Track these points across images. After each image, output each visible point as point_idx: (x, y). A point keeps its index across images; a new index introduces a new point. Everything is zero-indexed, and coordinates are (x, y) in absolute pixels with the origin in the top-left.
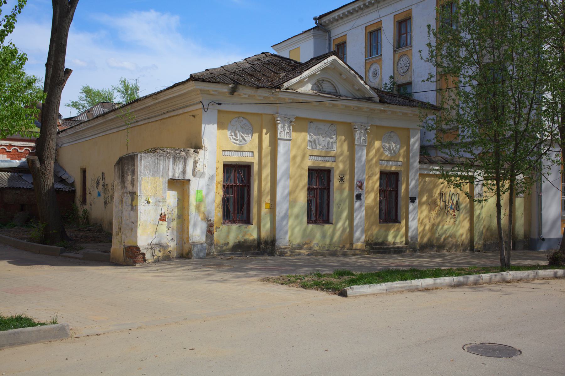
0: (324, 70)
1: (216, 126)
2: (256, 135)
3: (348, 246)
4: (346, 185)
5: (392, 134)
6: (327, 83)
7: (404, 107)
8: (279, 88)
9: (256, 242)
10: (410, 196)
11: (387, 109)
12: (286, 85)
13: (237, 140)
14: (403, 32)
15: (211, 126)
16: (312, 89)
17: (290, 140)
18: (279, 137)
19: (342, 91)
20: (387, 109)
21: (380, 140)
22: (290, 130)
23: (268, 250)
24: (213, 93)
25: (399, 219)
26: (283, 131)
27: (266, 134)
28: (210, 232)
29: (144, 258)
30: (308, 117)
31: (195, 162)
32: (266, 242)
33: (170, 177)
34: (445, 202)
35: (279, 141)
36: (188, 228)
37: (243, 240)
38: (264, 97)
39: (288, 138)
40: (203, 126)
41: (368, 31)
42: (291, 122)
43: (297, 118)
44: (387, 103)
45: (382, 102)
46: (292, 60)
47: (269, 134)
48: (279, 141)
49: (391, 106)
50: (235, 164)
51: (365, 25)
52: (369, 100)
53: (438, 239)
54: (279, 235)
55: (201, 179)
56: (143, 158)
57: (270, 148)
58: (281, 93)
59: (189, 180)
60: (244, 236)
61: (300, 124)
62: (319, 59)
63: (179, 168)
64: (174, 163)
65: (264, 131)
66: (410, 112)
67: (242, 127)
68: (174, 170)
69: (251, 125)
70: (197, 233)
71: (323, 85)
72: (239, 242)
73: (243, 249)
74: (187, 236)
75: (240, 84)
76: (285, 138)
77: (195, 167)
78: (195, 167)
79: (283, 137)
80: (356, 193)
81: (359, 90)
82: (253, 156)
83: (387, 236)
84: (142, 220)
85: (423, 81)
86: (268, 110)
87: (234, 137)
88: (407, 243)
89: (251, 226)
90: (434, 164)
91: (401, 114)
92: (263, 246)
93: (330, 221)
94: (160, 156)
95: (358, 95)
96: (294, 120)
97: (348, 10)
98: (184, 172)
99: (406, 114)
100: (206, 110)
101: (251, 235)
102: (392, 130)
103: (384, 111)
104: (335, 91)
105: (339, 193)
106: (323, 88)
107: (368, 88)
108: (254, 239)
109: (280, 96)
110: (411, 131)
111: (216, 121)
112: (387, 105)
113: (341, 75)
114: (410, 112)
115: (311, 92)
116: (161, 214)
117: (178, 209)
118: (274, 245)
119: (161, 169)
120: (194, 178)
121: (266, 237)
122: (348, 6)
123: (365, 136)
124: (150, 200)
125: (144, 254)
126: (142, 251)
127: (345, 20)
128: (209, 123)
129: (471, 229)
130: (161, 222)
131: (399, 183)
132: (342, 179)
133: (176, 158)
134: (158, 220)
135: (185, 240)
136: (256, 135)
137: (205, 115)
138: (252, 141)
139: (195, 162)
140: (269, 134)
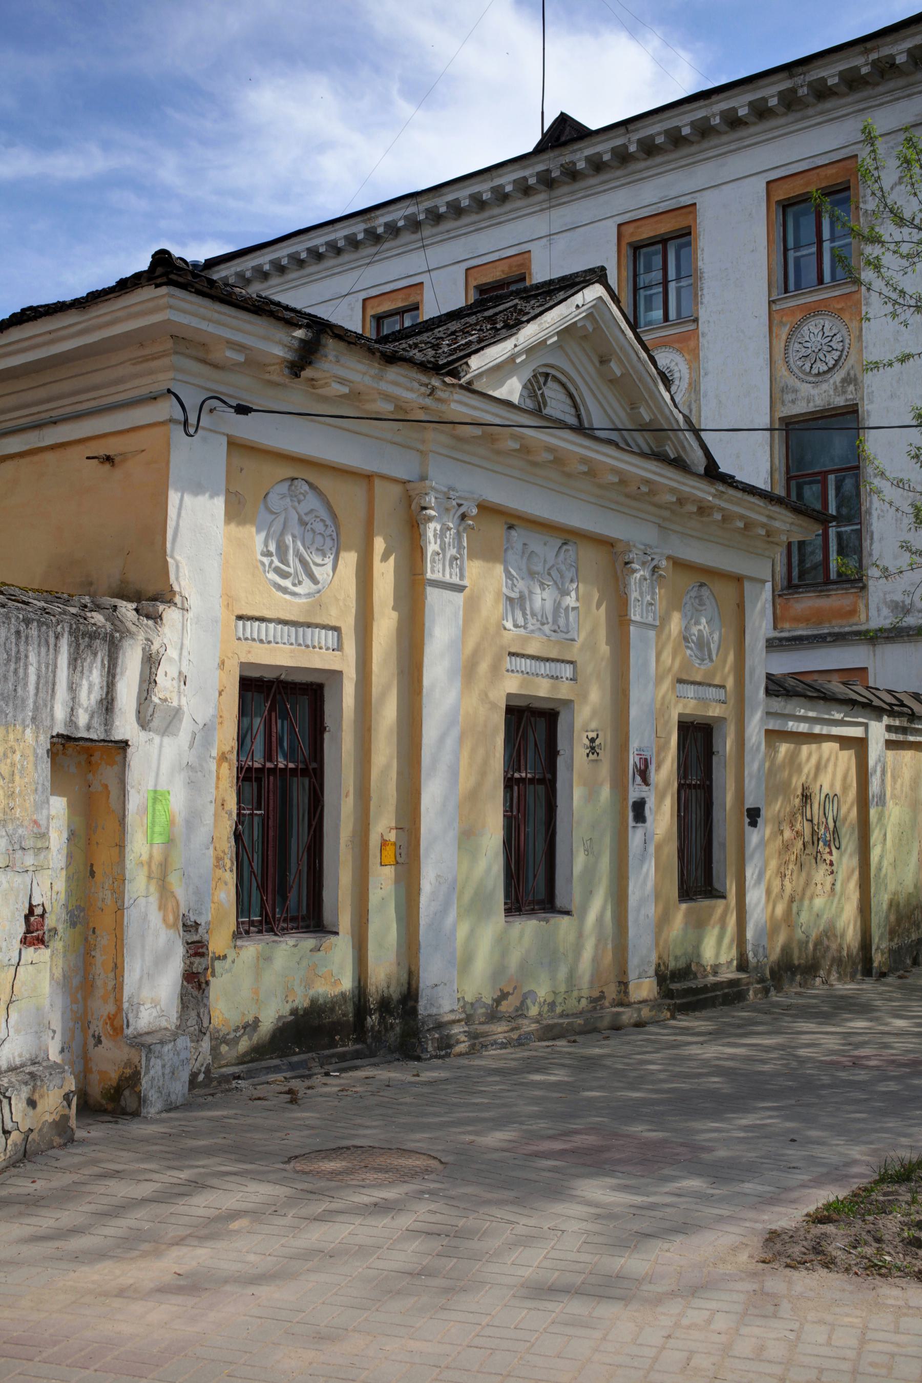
0: (568, 332)
1: (219, 503)
2: (116, 768)
3: (611, 992)
4: (605, 770)
5: (705, 592)
9: (350, 1009)
10: (747, 806)
13: (284, 575)
14: (670, 279)
15: (203, 500)
17: (460, 589)
18: (429, 575)
19: (597, 418)
22: (460, 547)
23: (392, 1037)
25: (716, 885)
27: (385, 558)
28: (195, 982)
31: (151, 662)
32: (385, 1005)
33: (60, 728)
34: (811, 821)
35: (430, 590)
37: (306, 1004)
39: (456, 580)
40: (173, 497)
41: (371, 312)
42: (463, 517)
43: (486, 509)
47: (392, 560)
48: (430, 590)
50: (269, 675)
51: (364, 295)
53: (803, 944)
54: (431, 972)
55: (166, 740)
60: (308, 985)
61: (495, 525)
64: (74, 662)
65: (379, 544)
67: (303, 523)
68: (69, 695)
69: (334, 516)
70: (152, 991)
72: (294, 1012)
73: (312, 1036)
74: (111, 1008)
76: (447, 578)
77: (148, 682)
78: (148, 682)
79: (437, 576)
82: (339, 647)
83: (697, 947)
87: (277, 563)
88: (742, 966)
89: (333, 938)
90: (795, 700)
92: (372, 1020)
93: (560, 902)
94: (27, 622)
96: (475, 511)
97: (310, 244)
98: (107, 705)
100: (191, 430)
101: (337, 982)
102: (706, 575)
103: (703, 510)
105: (584, 796)
108: (343, 994)
110: (747, 585)
111: (223, 488)
114: (764, 519)
116: (31, 908)
117: (68, 879)
118: (414, 1012)
119: (31, 688)
120: (144, 735)
122: (312, 234)
123: (654, 593)
127: (387, 245)
128: (197, 489)
130: (30, 953)
133: (84, 639)
134: (16, 944)
135: (98, 1026)
137: (185, 454)
138: (338, 575)
139: (151, 662)
140: (392, 560)
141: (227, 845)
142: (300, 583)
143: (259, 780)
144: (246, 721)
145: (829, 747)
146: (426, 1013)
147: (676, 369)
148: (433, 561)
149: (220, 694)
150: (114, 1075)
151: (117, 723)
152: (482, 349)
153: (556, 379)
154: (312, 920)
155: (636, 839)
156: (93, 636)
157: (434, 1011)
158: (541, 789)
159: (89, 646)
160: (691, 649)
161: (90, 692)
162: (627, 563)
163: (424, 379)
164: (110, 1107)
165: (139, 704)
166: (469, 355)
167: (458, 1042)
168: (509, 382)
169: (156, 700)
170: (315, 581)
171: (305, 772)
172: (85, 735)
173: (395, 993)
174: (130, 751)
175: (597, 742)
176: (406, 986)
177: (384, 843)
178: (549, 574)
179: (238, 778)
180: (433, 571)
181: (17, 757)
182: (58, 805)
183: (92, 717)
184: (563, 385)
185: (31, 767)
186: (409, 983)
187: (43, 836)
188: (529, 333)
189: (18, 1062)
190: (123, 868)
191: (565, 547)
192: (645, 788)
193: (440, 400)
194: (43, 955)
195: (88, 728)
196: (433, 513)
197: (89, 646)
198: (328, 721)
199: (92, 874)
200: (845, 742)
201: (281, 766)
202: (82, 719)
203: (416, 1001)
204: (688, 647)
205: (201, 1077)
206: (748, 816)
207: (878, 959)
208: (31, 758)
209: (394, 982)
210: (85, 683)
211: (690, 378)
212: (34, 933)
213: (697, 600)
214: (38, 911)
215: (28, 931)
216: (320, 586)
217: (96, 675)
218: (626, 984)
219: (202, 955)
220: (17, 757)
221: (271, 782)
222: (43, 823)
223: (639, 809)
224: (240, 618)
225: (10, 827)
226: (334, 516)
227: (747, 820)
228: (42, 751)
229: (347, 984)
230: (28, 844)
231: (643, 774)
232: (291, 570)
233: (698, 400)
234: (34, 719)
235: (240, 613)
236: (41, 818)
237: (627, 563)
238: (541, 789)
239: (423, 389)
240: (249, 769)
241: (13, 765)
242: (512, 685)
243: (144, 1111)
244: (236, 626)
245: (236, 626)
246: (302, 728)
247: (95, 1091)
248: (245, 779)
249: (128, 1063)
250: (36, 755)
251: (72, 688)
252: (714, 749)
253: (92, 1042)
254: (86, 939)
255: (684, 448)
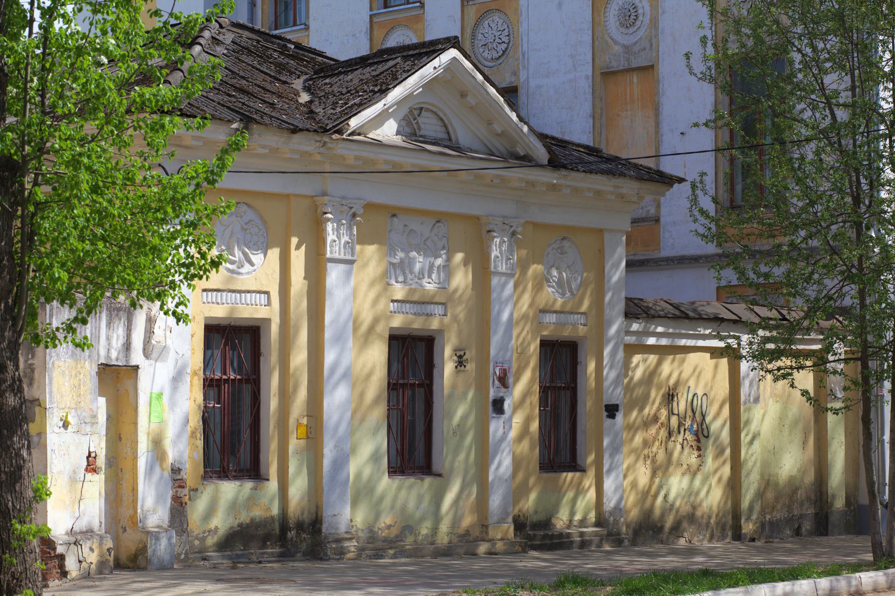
0: (429, 85)
2: (274, 254)
5: (566, 244)
6: (429, 114)
7: (599, 177)
8: (340, 132)
9: (277, 526)
10: (605, 403)
11: (563, 182)
12: (354, 123)
16: (398, 133)
18: (328, 255)
20: (563, 182)
21: (379, 243)
22: (351, 235)
23: (304, 546)
24: (194, 143)
25: (579, 462)
26: (335, 238)
29: (62, 566)
30: (465, 210)
32: (300, 526)
35: (329, 265)
36: (134, 490)
37: (248, 521)
38: (304, 154)
39: (349, 257)
42: (354, 215)
43: (370, 207)
44: (564, 167)
45: (554, 164)
46: (290, 41)
47: (303, 247)
48: (329, 265)
49: (574, 174)
52: (526, 160)
55: (158, 364)
56: (54, 312)
57: (306, 282)
58: (342, 145)
59: (137, 368)
61: (377, 223)
62: (420, 56)
63: (118, 337)
64: (109, 325)
65: (294, 241)
66: (612, 189)
69: (265, 223)
70: (152, 504)
71: (420, 120)
74: (131, 512)
75: (258, 123)
77: (149, 332)
79: (336, 256)
80: (492, 394)
81: (503, 135)
82: (269, 304)
84: (54, 471)
85: (696, 125)
86: (305, 186)
89: (266, 483)
90: (657, 320)
91: (591, 194)
92: (291, 534)
93: (435, 467)
95: (498, 145)
98: (127, 346)
99: (598, 193)
102: (566, 233)
103: (553, 188)
104: (445, 136)
106: (419, 129)
107: (525, 129)
108: (272, 517)
109: (339, 152)
110: (607, 237)
112: (564, 172)
113: (463, 95)
114: (612, 189)
115: (398, 140)
116: (90, 453)
117: (107, 441)
118: (319, 531)
121: (298, 513)
124: (70, 419)
125: (62, 557)
126: (60, 550)
129: (734, 485)
130: (89, 476)
131: (579, 368)
132: (461, 362)
134: (83, 471)
136: (274, 254)
140: (303, 247)
141: (196, 421)
142: (242, 266)
143: (219, 386)
144: (209, 352)
145: (693, 357)
146: (327, 532)
147: (640, 5)
148: (331, 246)
149: (192, 336)
150: (133, 548)
151: (132, 356)
152: (360, 112)
153: (428, 110)
154: (253, 471)
155: (496, 426)
156: (119, 310)
157: (333, 531)
158: (422, 390)
159: (117, 315)
160: (553, 287)
161: (117, 340)
162: (489, 231)
163: (318, 138)
164: (131, 565)
165: (145, 345)
166: (350, 118)
167: (349, 552)
168: (387, 123)
169: (153, 342)
170: (252, 264)
171: (247, 381)
172: (116, 363)
173: (307, 518)
174: (140, 371)
175: (465, 358)
176: (314, 515)
177: (299, 425)
178: (425, 244)
179: (204, 385)
180: (331, 253)
181: (82, 376)
182: (102, 401)
183: (119, 353)
184: (435, 113)
185: (88, 381)
186: (317, 513)
187: (95, 416)
188: (396, 93)
189: (84, 529)
190: (137, 436)
191: (438, 224)
192: (503, 390)
193: (330, 148)
194: (95, 477)
195: (117, 359)
196: (330, 216)
197: (117, 315)
198: (263, 349)
199: (120, 439)
200: (715, 353)
201: (232, 377)
202: (114, 354)
203: (321, 524)
204: (549, 286)
205: (183, 556)
206: (606, 410)
207: (748, 528)
208: (89, 377)
209: (306, 513)
210: (115, 335)
211: (651, 15)
212: (91, 467)
213: (559, 251)
214: (93, 455)
215: (88, 465)
216: (255, 267)
217: (121, 331)
218: (487, 527)
219: (183, 487)
220: (82, 376)
221: (226, 388)
222: (95, 410)
223: (498, 406)
224: (204, 290)
225: (79, 412)
226: (265, 223)
227: (605, 414)
228: (94, 373)
229: (275, 511)
230: (88, 420)
231: (503, 380)
232: (237, 259)
233: (657, 36)
234: (89, 356)
235: (205, 287)
236: (94, 407)
237: (489, 231)
238: (568, 393)
239: (318, 144)
240: (212, 380)
241: (80, 380)
242: (397, 322)
243: (149, 567)
244: (202, 296)
245: (202, 296)
246: (245, 355)
247: (123, 558)
248: (392, 389)
249: (141, 541)
250: (91, 375)
251: (108, 339)
252: (579, 360)
253: (121, 530)
254: (117, 475)
255: (530, 148)
